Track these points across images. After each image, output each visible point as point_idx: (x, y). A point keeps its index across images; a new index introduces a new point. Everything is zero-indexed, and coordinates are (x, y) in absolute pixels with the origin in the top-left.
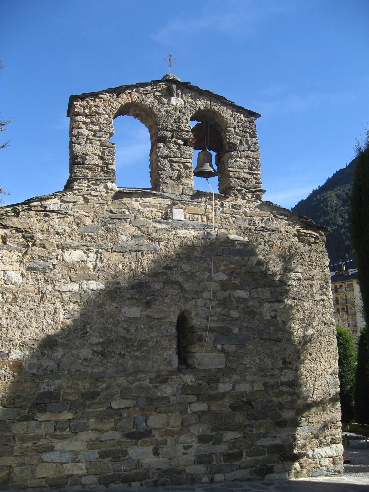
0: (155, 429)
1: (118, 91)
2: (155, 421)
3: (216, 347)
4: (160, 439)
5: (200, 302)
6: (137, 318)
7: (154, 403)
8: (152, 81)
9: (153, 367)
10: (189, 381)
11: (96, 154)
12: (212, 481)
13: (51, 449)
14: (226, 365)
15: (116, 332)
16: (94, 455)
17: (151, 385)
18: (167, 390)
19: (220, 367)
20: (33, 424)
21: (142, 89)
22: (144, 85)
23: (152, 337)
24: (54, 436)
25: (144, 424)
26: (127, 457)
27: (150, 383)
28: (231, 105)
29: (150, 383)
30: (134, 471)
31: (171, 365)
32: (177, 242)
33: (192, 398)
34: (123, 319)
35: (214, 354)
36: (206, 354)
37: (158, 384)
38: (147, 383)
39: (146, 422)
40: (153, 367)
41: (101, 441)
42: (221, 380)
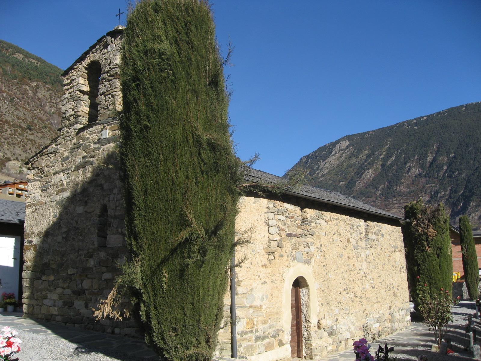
0: (87, 290)
1: (82, 59)
2: (86, 284)
3: (118, 230)
4: (89, 297)
5: (112, 197)
6: (255, 195)
7: (85, 272)
8: (97, 41)
9: (86, 246)
10: (102, 256)
11: (70, 109)
12: (113, 332)
13: (46, 297)
14: (123, 245)
15: (72, 224)
16: (60, 303)
17: (85, 259)
18: (92, 263)
19: (119, 245)
20: (40, 281)
21: (94, 49)
22: (94, 46)
23: (87, 226)
24: (48, 290)
25: (80, 285)
26: (73, 307)
27: (84, 257)
28: (87, 53)
29: (84, 257)
30: (76, 317)
31: (94, 245)
32: (105, 153)
33: (104, 269)
34: (76, 215)
35: (117, 236)
36: (112, 236)
37: (88, 259)
38: (83, 257)
39: (82, 284)
40: (86, 246)
41: (64, 295)
42: (119, 256)
